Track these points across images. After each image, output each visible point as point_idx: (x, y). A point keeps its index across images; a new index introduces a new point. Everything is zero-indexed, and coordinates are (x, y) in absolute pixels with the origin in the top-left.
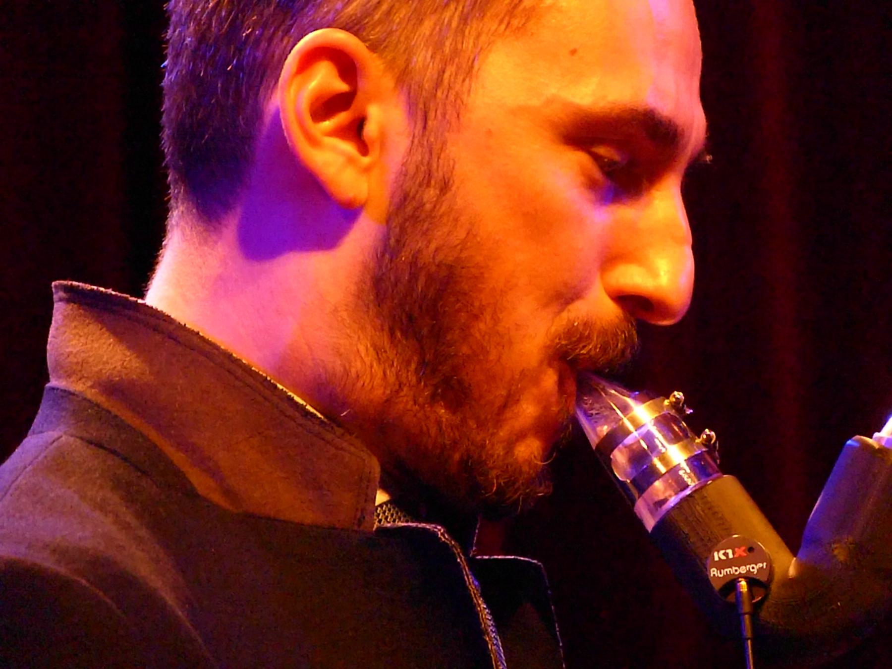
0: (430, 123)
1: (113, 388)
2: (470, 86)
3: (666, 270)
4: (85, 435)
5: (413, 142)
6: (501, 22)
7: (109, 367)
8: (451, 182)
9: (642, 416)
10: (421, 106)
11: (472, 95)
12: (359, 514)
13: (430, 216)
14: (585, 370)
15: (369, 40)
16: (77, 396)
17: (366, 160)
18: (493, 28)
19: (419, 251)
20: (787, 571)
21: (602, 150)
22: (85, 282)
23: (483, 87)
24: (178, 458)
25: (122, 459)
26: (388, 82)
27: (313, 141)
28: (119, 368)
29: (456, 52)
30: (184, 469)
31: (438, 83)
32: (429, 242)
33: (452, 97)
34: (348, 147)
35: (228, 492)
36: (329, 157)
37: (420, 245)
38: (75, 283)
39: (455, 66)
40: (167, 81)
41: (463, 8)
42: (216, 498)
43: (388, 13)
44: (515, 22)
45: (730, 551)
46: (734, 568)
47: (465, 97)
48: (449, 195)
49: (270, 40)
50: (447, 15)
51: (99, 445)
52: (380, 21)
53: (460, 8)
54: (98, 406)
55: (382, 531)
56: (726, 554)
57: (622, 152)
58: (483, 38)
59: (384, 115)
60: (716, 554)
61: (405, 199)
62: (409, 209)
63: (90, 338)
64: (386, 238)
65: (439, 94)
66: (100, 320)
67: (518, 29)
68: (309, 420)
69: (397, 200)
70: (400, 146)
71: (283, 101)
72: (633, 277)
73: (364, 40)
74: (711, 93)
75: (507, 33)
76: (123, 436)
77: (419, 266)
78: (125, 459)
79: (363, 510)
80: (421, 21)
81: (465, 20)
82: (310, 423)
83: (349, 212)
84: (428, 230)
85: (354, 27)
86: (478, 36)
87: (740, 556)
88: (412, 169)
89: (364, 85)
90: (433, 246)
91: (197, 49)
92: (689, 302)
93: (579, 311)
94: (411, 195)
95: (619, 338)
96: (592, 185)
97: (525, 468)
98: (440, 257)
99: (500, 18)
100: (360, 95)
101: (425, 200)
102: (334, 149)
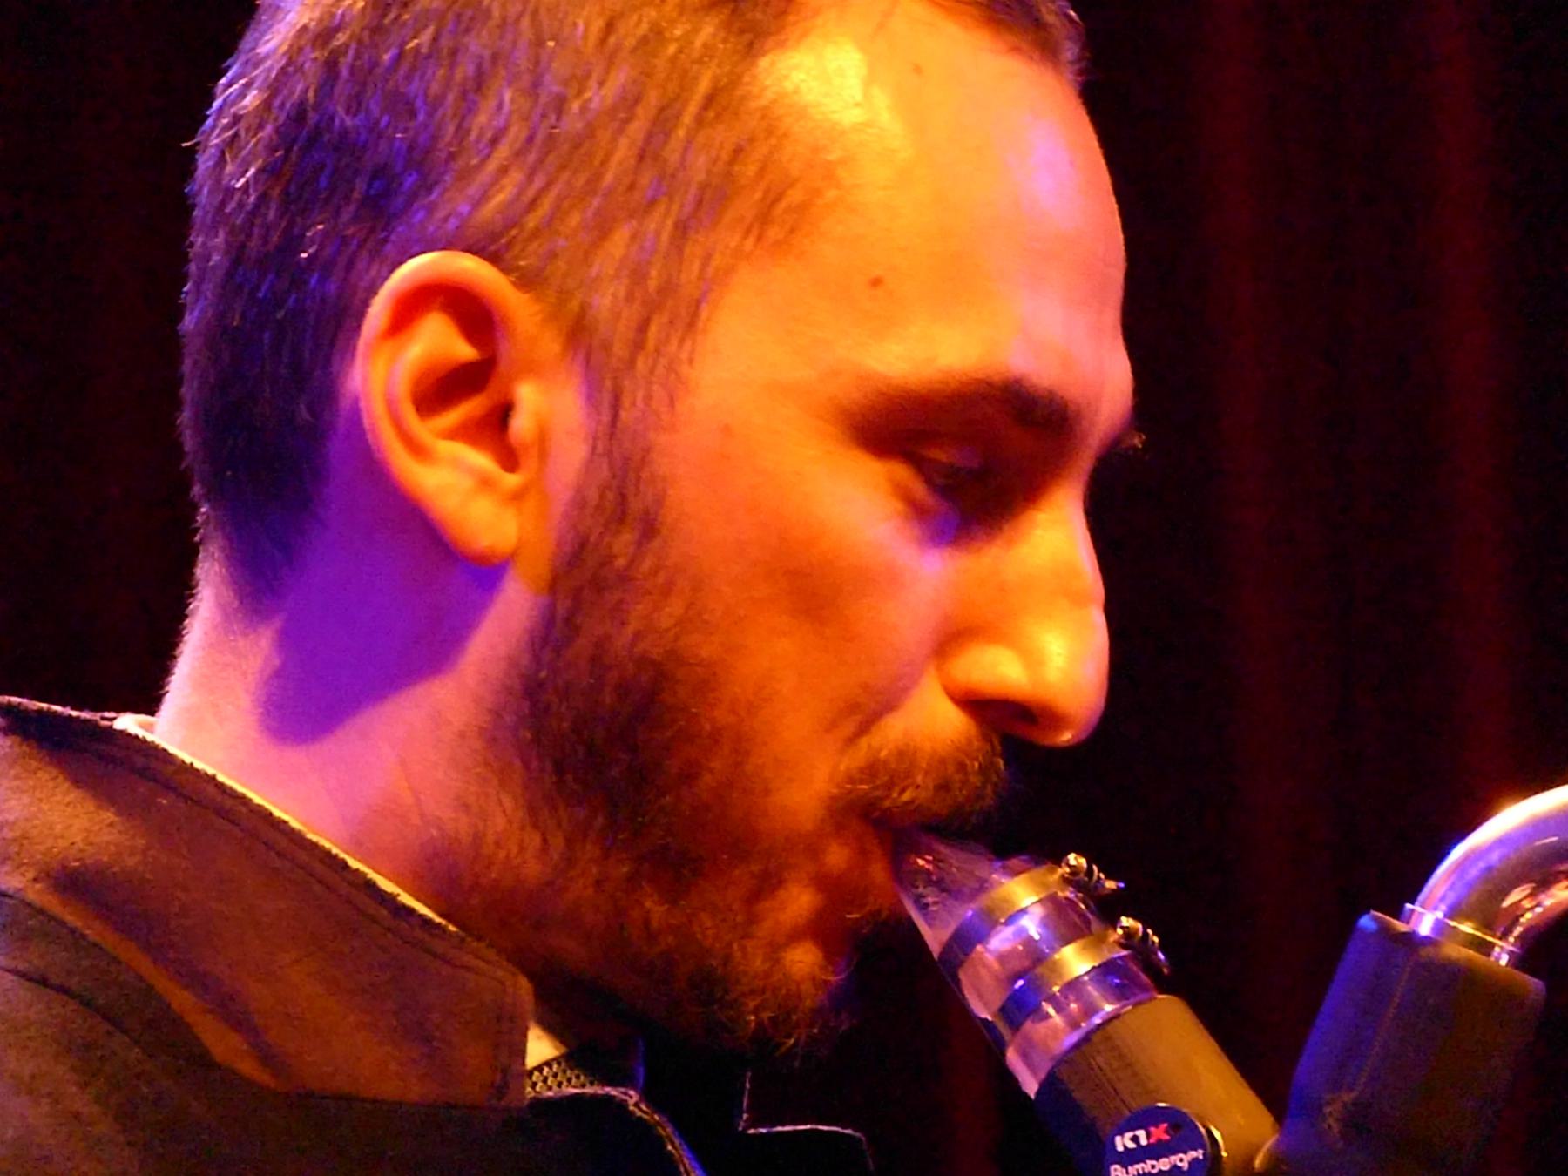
0: (623, 414)
1: (73, 881)
3: (1059, 654)
4: (22, 967)
5: (594, 448)
6: (748, 232)
7: (62, 843)
9: (1023, 898)
10: (608, 384)
12: (498, 1077)
13: (625, 578)
14: (912, 827)
15: (518, 268)
16: (11, 897)
17: (512, 480)
18: (733, 244)
19: (608, 637)
20: (1251, 1159)
21: (940, 455)
22: (32, 698)
24: (182, 999)
25: (81, 1002)
26: (550, 345)
27: (418, 450)
28: (81, 845)
30: (189, 1019)
31: (638, 345)
33: (660, 370)
34: (481, 460)
35: (266, 1057)
36: (448, 477)
38: (15, 700)
40: (189, 322)
41: (682, 206)
42: (248, 1067)
43: (550, 220)
44: (773, 233)
45: (1141, 1134)
46: (1150, 1162)
47: (684, 369)
48: (656, 543)
49: (350, 266)
51: (43, 982)
52: (536, 234)
53: (675, 207)
54: (41, 911)
55: (539, 1104)
56: (1135, 1139)
58: (717, 261)
59: (544, 402)
60: (1118, 1139)
63: (37, 794)
64: (551, 609)
65: (641, 364)
66: (60, 764)
69: (568, 549)
70: (571, 456)
71: (365, 379)
72: (999, 669)
73: (505, 270)
76: (85, 963)
78: (87, 1004)
79: (504, 1071)
81: (683, 229)
83: (486, 573)
85: (487, 248)
86: (707, 258)
87: (1159, 1141)
88: (593, 495)
89: (508, 353)
90: (630, 630)
91: (230, 274)
93: (894, 730)
94: (592, 539)
95: (969, 769)
96: (917, 511)
97: (807, 987)
98: (641, 647)
100: (502, 367)
101: (615, 549)
102: (457, 464)
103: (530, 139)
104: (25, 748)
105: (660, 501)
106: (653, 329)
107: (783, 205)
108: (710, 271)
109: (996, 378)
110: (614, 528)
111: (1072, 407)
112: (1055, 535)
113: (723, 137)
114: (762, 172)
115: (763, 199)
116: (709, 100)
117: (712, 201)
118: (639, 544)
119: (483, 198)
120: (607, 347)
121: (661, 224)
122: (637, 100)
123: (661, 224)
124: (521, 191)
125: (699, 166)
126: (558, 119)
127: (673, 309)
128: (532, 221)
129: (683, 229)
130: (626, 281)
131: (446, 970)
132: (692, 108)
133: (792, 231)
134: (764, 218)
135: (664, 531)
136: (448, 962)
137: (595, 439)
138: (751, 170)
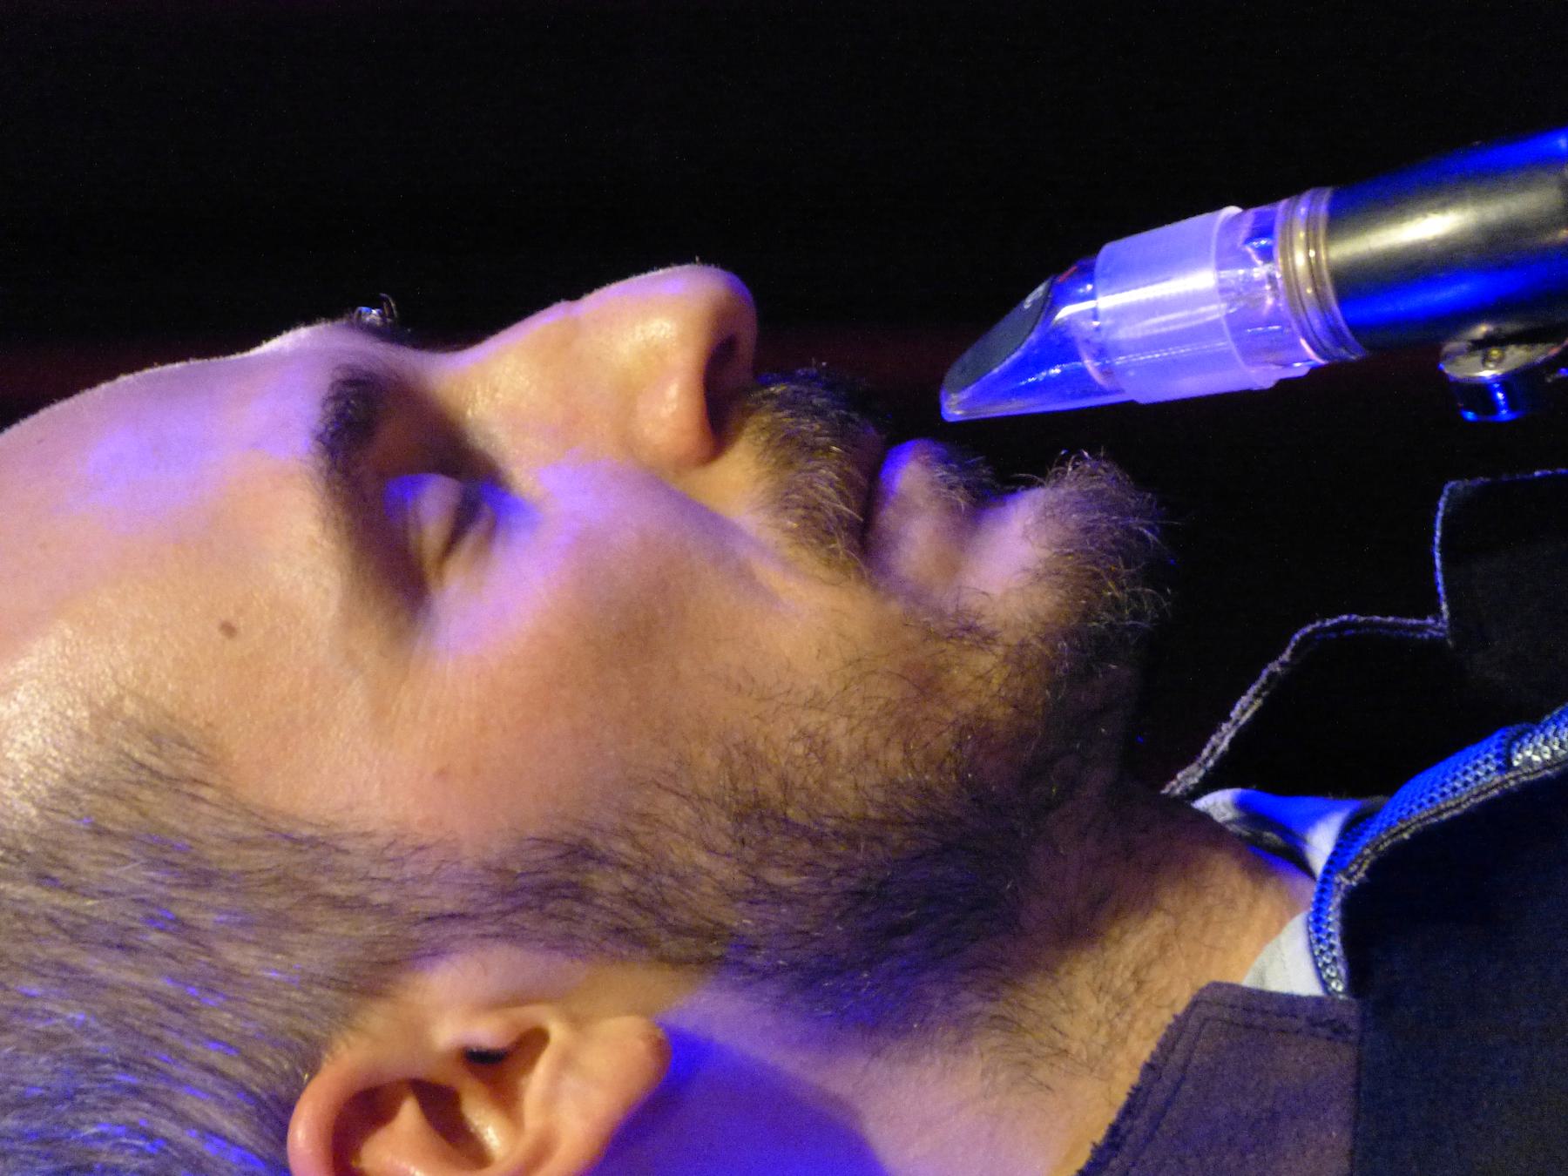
0: (449, 907)
2: (356, 835)
3: (649, 329)
6: (195, 798)
8: (567, 839)
10: (416, 933)
11: (370, 829)
17: (557, 1031)
18: (215, 812)
23: (350, 808)
26: (377, 1018)
29: (281, 880)
32: (698, 868)
33: (384, 871)
34: (537, 1082)
37: (709, 890)
39: (315, 878)
44: (191, 767)
47: (379, 842)
50: (207, 919)
57: (404, 489)
58: (238, 829)
59: (451, 1008)
61: (619, 931)
62: (639, 920)
64: (705, 962)
65: (381, 898)
67: (203, 758)
68: (1124, 1138)
72: (670, 407)
73: (298, 1089)
74: (228, 327)
75: (217, 780)
77: (751, 885)
79: (1312, 1022)
80: (231, 974)
81: (204, 878)
82: (1130, 1138)
83: (683, 1062)
84: (672, 875)
86: (240, 841)
92: (737, 280)
99: (189, 803)
100: (421, 1070)
102: (550, 1100)
103: (135, 1091)
104: (769, 1021)
105: (546, 842)
106: (337, 890)
107: (152, 761)
108: (252, 833)
109: (322, 463)
110: (558, 894)
111: (339, 375)
112: (500, 384)
113: (87, 861)
114: (117, 796)
115: (152, 787)
116: (43, 879)
117: (163, 851)
118: (602, 860)
119: (212, 1134)
120: (370, 945)
121: (205, 910)
122: (61, 966)
123: (205, 910)
124: (194, 1090)
125: (134, 876)
126: (105, 1061)
127: (301, 872)
128: (239, 1069)
129: (204, 878)
130: (286, 937)
131: (1187, 1087)
132: (58, 899)
133: (182, 742)
134: (172, 783)
135: (581, 832)
136: (1177, 1088)
137: (484, 936)
138: (120, 810)
